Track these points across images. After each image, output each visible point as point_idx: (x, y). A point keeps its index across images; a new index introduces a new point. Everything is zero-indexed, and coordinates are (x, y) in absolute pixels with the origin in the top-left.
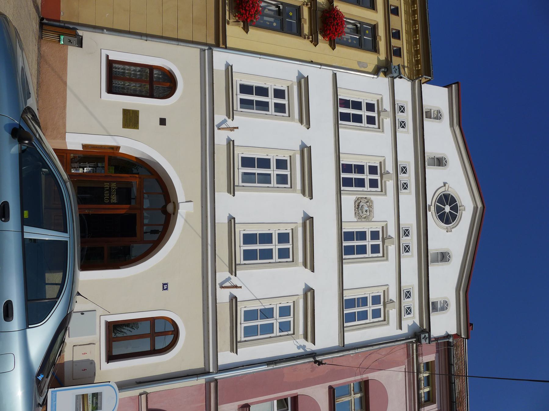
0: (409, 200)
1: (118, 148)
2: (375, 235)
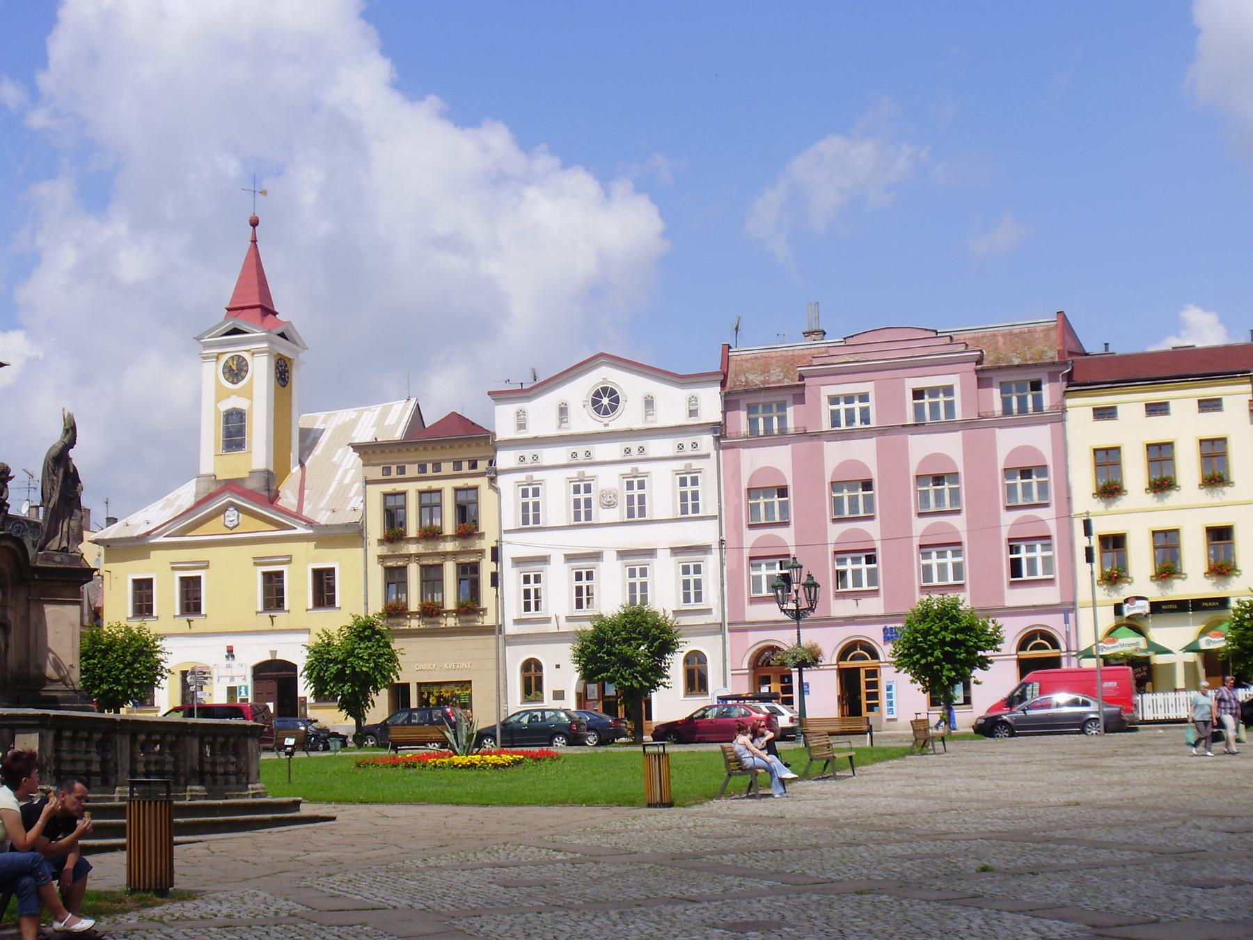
0: (603, 451)
1: (316, 547)
2: (630, 486)
